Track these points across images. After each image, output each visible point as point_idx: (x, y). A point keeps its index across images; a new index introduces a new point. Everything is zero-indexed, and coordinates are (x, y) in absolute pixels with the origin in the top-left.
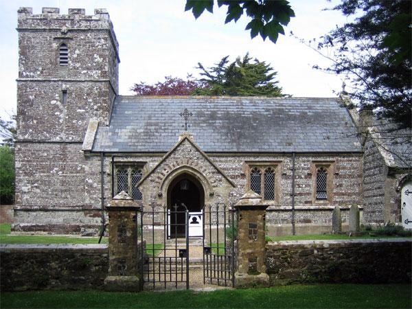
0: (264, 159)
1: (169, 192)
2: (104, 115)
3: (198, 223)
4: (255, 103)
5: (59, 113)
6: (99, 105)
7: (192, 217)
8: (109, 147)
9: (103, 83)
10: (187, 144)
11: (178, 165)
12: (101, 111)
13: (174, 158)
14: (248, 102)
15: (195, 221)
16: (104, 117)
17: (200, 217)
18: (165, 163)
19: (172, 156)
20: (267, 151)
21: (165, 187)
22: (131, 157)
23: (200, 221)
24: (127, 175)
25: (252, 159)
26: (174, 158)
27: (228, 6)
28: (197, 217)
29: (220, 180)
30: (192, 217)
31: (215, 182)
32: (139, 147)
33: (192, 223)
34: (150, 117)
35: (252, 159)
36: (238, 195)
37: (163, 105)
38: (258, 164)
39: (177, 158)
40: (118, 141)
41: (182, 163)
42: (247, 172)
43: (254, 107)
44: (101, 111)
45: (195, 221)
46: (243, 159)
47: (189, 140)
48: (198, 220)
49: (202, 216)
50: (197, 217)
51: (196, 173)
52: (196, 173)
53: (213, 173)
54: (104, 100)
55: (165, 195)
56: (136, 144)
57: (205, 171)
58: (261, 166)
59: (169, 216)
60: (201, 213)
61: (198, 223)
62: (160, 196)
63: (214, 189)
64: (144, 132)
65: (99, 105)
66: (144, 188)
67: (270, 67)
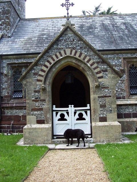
2: (6, 29)
3: (84, 119)
4: (123, 17)
6: (3, 21)
7: (59, 113)
8: (6, 51)
9: (6, 3)
10: (70, 35)
11: (61, 56)
12: (5, 25)
13: (57, 49)
16: (6, 30)
17: (86, 113)
18: (47, 54)
19: (55, 47)
21: (50, 80)
22: (24, 58)
23: (87, 117)
25: (129, 56)
26: (57, 49)
29: (106, 71)
30: (59, 113)
32: (32, 50)
33: (59, 120)
34: (43, 30)
35: (129, 56)
36: (119, 90)
37: (54, 22)
39: (60, 49)
42: (126, 68)
43: (124, 20)
44: (5, 25)
46: (121, 56)
47: (71, 30)
48: (84, 116)
49: (89, 112)
51: (79, 64)
52: (79, 64)
53: (98, 63)
54: (7, 17)
55: (49, 89)
56: (29, 48)
57: (90, 64)
60: (88, 107)
61: (84, 119)
62: (44, 90)
63: (100, 80)
64: (37, 40)
65: (3, 21)
66: (27, 82)
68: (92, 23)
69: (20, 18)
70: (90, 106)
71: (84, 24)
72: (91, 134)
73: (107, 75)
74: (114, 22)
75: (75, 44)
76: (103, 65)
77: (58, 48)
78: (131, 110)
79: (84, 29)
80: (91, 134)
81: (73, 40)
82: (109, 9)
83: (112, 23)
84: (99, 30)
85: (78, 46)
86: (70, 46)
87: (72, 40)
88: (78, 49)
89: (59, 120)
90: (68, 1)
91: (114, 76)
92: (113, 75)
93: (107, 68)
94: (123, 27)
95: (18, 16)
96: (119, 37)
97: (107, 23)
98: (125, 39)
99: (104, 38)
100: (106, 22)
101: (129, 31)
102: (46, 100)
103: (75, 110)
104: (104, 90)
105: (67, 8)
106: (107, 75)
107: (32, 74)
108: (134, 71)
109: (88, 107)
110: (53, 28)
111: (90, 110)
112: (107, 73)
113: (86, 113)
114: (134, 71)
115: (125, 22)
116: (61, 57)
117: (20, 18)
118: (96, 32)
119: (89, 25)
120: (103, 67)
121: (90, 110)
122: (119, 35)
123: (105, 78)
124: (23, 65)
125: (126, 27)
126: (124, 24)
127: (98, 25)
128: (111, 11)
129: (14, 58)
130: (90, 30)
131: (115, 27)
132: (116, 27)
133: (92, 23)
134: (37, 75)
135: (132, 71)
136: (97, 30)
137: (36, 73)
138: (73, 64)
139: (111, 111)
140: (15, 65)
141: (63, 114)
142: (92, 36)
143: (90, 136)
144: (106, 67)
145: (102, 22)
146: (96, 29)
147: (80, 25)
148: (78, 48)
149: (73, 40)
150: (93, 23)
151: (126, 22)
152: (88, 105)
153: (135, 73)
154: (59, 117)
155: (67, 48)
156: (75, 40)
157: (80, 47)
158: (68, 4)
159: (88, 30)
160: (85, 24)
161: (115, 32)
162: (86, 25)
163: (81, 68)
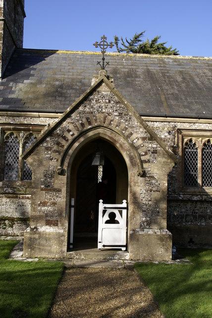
0: (203, 127)
1: (73, 166)
3: (117, 222)
5: (46, 144)
7: (109, 211)
11: (90, 123)
14: (171, 61)
15: (112, 220)
17: (121, 213)
20: (188, 128)
23: (122, 219)
24: (19, 143)
27: (93, 164)
28: (116, 212)
31: (146, 154)
33: (107, 222)
38: (195, 133)
40: (11, 96)
41: (96, 120)
45: (112, 220)
48: (118, 218)
49: (124, 212)
50: (116, 212)
58: (199, 136)
59: (73, 209)
60: (124, 205)
61: (117, 222)
67: (178, 53)
68: (130, 67)
69: (16, 46)
70: (127, 203)
71: (119, 67)
72: (126, 246)
73: (155, 158)
74: (165, 68)
75: (111, 107)
76: (150, 143)
77: (85, 112)
78: (183, 210)
79: (118, 75)
80: (126, 246)
81: (109, 102)
82: (154, 41)
83: (162, 70)
84: (141, 80)
85: (116, 111)
86: (104, 111)
87: (107, 101)
88: (116, 116)
89: (107, 222)
90: (105, 40)
91: (166, 160)
92: (164, 160)
93: (156, 148)
94: (179, 79)
95: (14, 42)
96: (172, 94)
97: (155, 69)
98: (181, 99)
99: (150, 94)
100: (152, 68)
101: (188, 86)
102: (62, 190)
103: (105, 208)
104: (149, 181)
105: (102, 50)
106: (155, 158)
107: (43, 148)
108: (192, 150)
109: (124, 205)
110: (69, 69)
111: (127, 208)
112: (156, 155)
113: (121, 213)
114: (192, 150)
115: (181, 70)
116: (90, 127)
117: (16, 46)
118: (137, 83)
119: (127, 70)
120: (150, 146)
121: (127, 208)
122: (172, 91)
123: (153, 162)
124: (22, 127)
125: (184, 78)
126: (181, 72)
127: (140, 71)
128: (159, 42)
129: (9, 115)
130: (128, 79)
131: (166, 77)
132: (168, 77)
133: (130, 67)
134: (50, 150)
135: (190, 150)
136: (138, 79)
137: (50, 147)
138: (107, 138)
139: (158, 212)
140: (9, 127)
141: (113, 213)
142: (132, 90)
143: (124, 249)
144: (155, 146)
145: (147, 66)
146: (137, 77)
147: (113, 68)
148: (116, 114)
149: (109, 102)
150: (133, 67)
151: (184, 70)
152: (125, 201)
153: (192, 153)
154: (106, 218)
155: (99, 113)
156: (112, 102)
157: (119, 113)
158: (105, 43)
159: (125, 79)
160: (121, 68)
161: (167, 85)
162: (122, 70)
163: (118, 145)
